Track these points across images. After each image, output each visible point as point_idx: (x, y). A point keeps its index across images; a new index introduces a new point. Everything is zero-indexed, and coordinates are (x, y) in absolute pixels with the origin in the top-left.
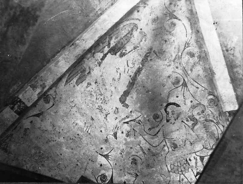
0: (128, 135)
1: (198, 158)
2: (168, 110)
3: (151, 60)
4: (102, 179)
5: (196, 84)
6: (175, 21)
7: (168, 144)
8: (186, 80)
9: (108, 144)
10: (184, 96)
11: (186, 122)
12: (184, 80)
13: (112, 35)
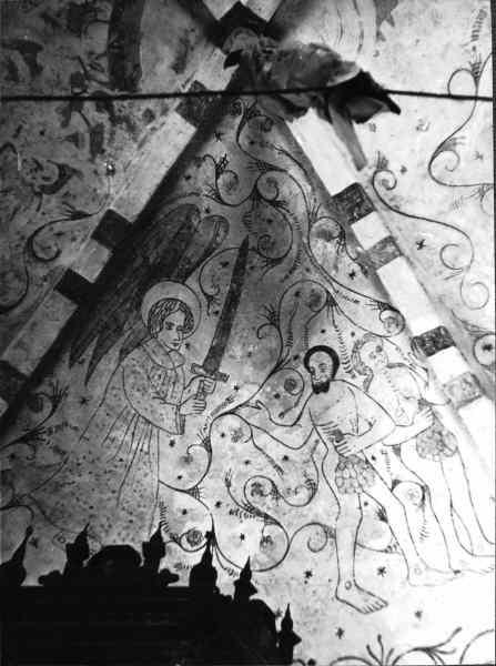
0: (235, 439)
1: (390, 450)
2: (311, 364)
3: (252, 268)
4: (191, 539)
5: (352, 295)
6: (274, 175)
7: (324, 437)
8: (331, 291)
9: (192, 465)
10: (336, 327)
11: (350, 380)
12: (328, 292)
13: (148, 239)
